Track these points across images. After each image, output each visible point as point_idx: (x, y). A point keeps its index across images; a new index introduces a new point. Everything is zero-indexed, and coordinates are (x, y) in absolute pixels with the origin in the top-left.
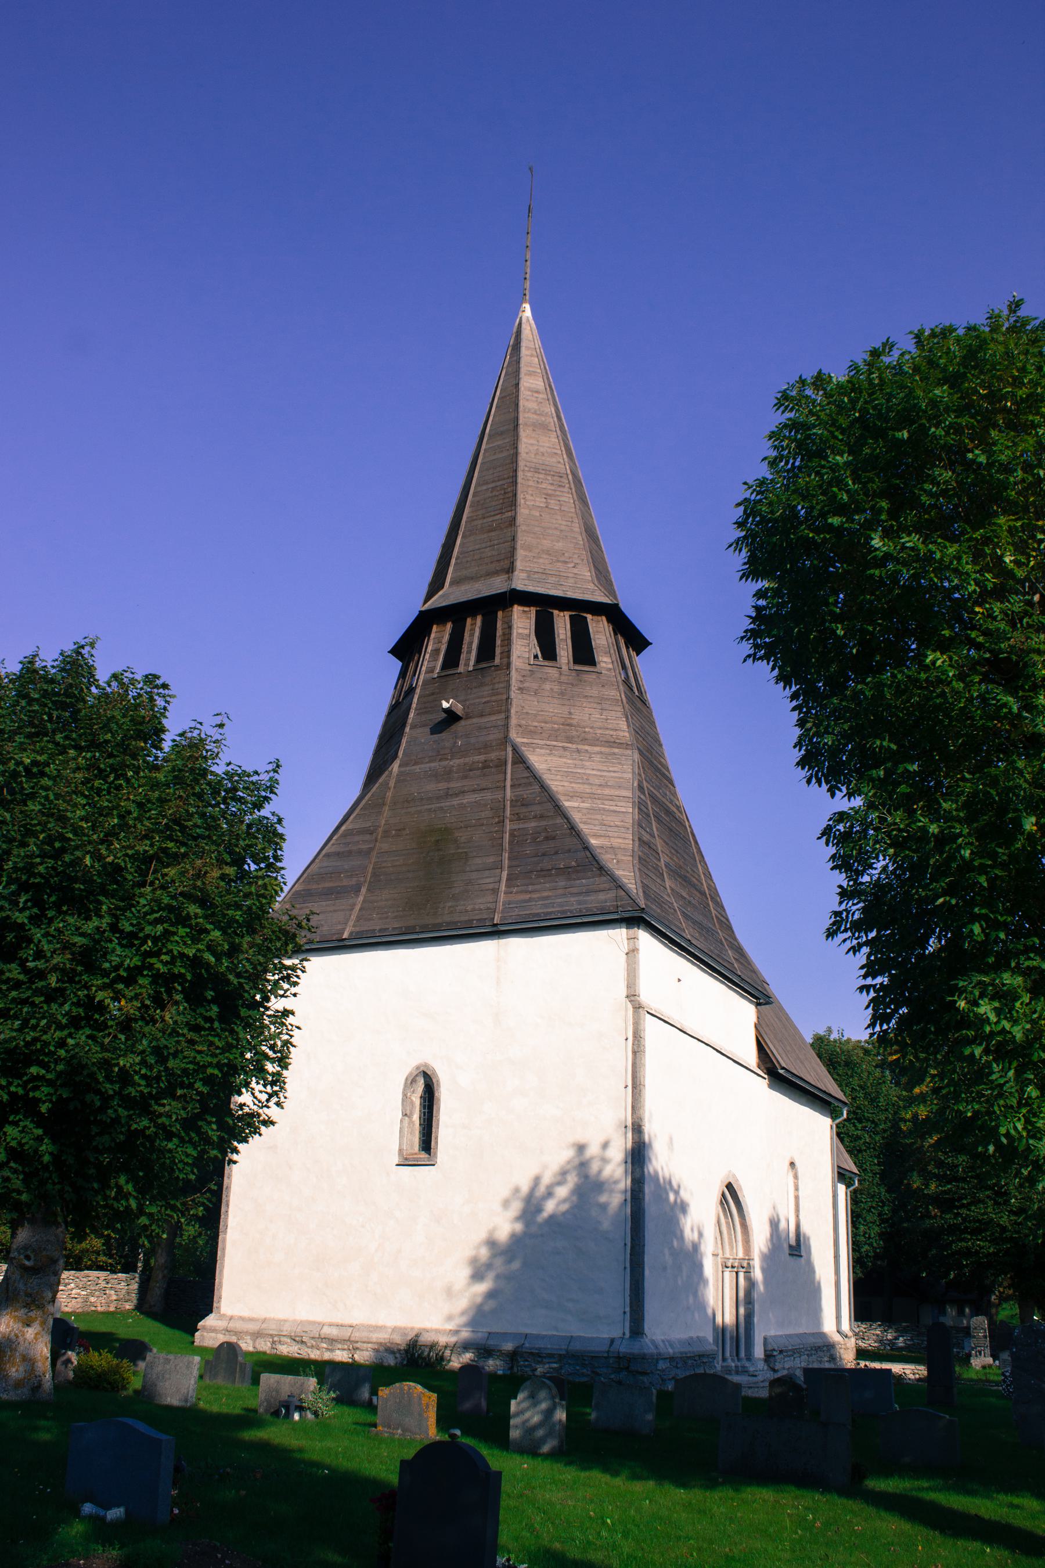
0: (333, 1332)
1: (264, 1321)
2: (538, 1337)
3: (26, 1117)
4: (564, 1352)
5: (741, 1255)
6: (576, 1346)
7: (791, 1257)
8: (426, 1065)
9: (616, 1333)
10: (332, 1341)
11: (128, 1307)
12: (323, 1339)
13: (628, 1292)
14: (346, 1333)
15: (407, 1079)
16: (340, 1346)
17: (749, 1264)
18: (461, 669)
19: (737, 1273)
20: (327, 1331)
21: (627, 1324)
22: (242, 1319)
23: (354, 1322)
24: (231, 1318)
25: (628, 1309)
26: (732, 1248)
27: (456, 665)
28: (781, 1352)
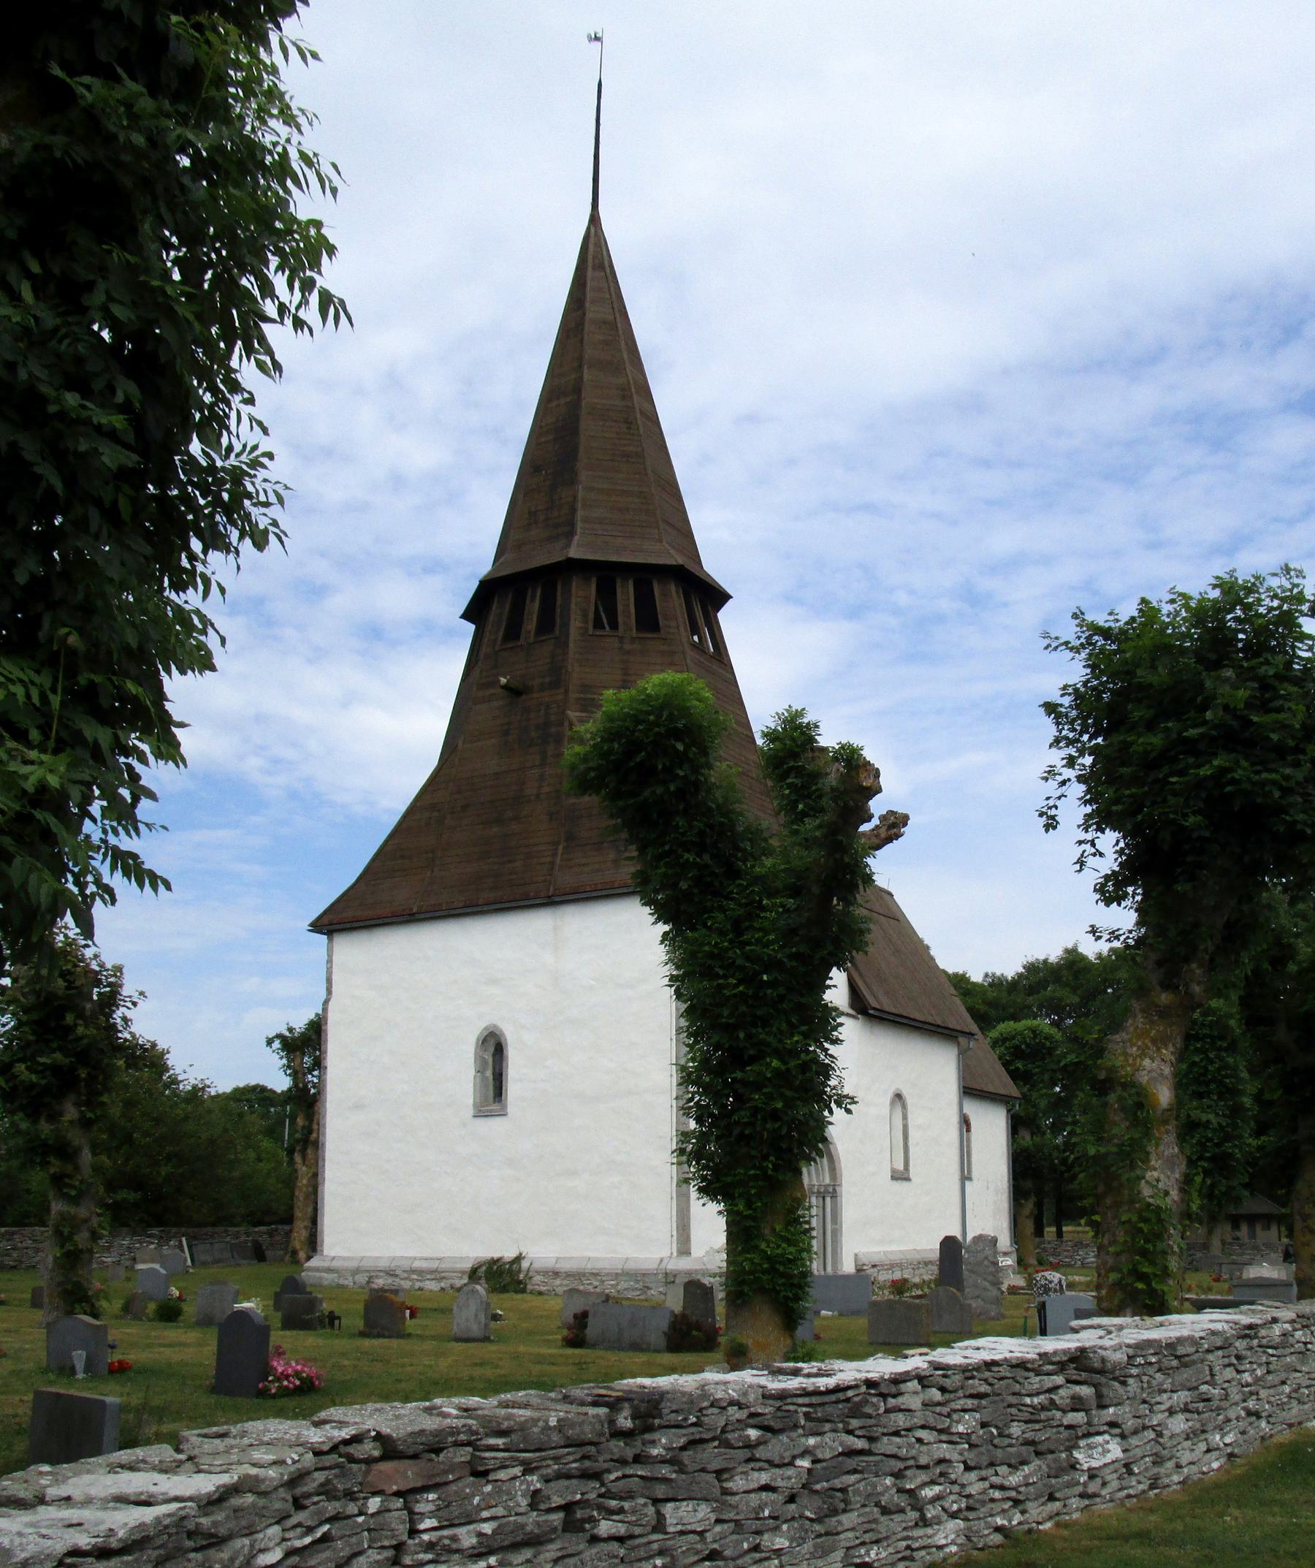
0: (424, 1265)
1: (362, 1258)
2: (597, 1259)
3: (699, 676)
4: (620, 1271)
5: (827, 1181)
6: (631, 1266)
7: (895, 1182)
8: (495, 1026)
9: (665, 1253)
10: (420, 1272)
11: (1215, 1465)
12: (413, 1271)
13: (674, 1219)
14: (434, 1265)
15: (478, 1040)
16: (429, 1277)
17: (834, 1190)
18: (522, 642)
19: (824, 1198)
20: (417, 1264)
21: (675, 1246)
22: (344, 1259)
23: (440, 1255)
24: (333, 1258)
25: (675, 1233)
26: (818, 1174)
27: (517, 637)
28: (874, 1266)
